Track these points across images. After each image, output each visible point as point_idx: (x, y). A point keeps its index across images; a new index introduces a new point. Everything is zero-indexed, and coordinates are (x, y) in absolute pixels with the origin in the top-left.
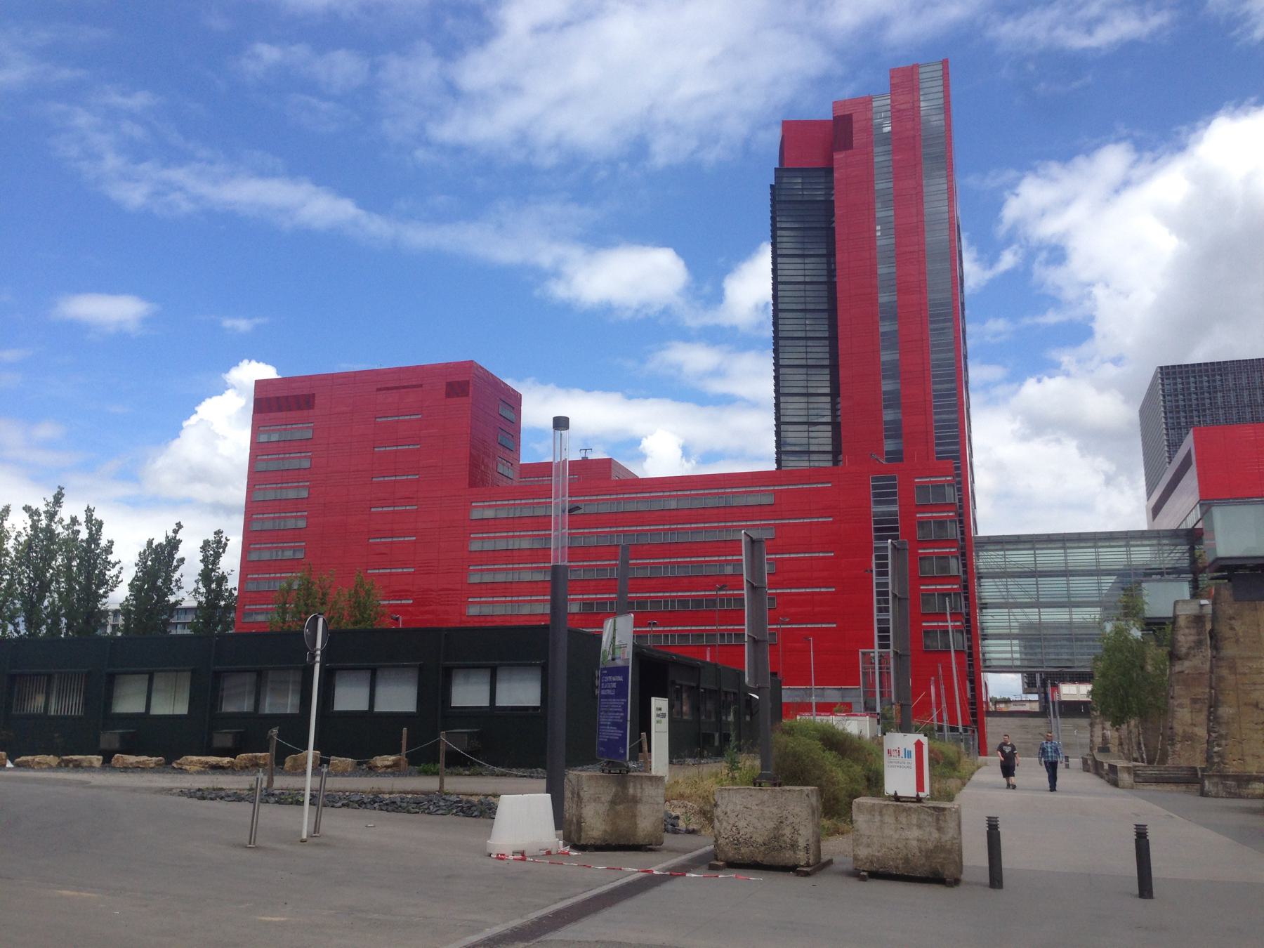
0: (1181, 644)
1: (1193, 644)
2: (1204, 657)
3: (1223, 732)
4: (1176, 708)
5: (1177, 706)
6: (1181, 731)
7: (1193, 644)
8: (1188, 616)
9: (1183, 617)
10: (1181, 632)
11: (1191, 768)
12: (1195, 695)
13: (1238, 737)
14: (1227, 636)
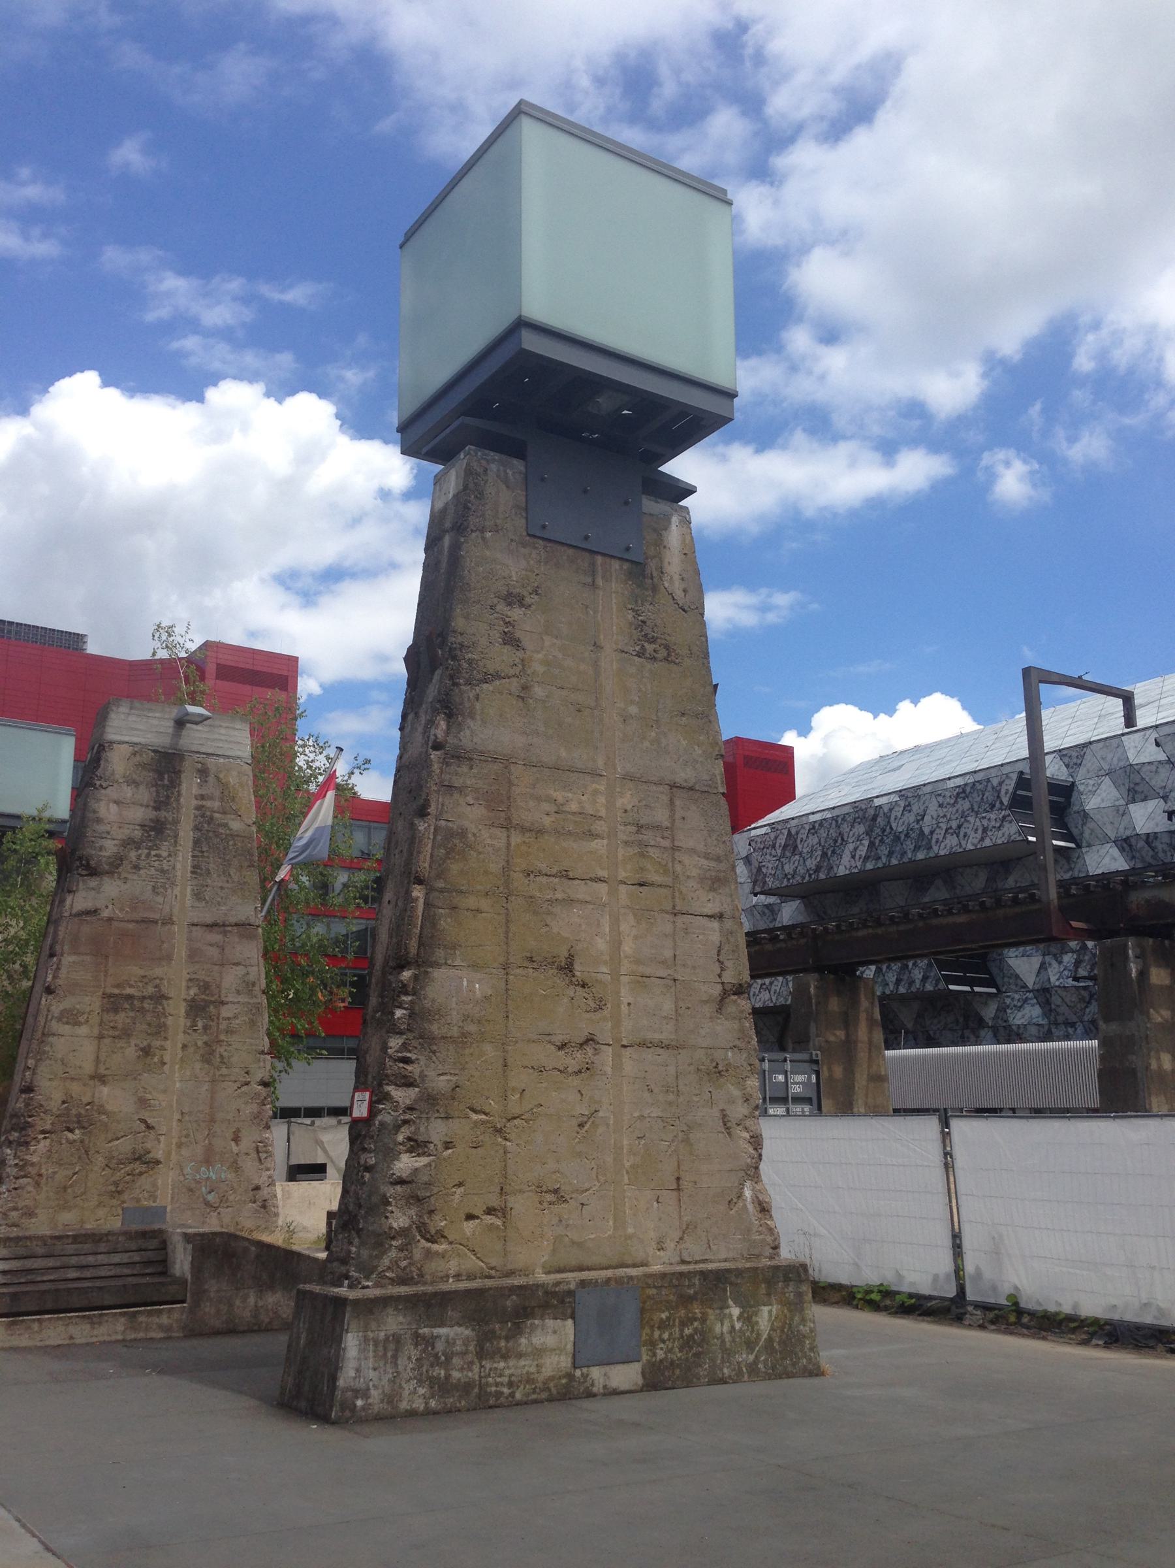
0: (101, 828)
1: (138, 834)
2: (163, 871)
3: (441, 1083)
4: (55, 1026)
5: (59, 1019)
6: (58, 1096)
7: (138, 834)
8: (137, 749)
9: (125, 750)
10: (112, 793)
11: (144, 1235)
12: (118, 986)
13: (493, 1105)
14: (491, 667)
